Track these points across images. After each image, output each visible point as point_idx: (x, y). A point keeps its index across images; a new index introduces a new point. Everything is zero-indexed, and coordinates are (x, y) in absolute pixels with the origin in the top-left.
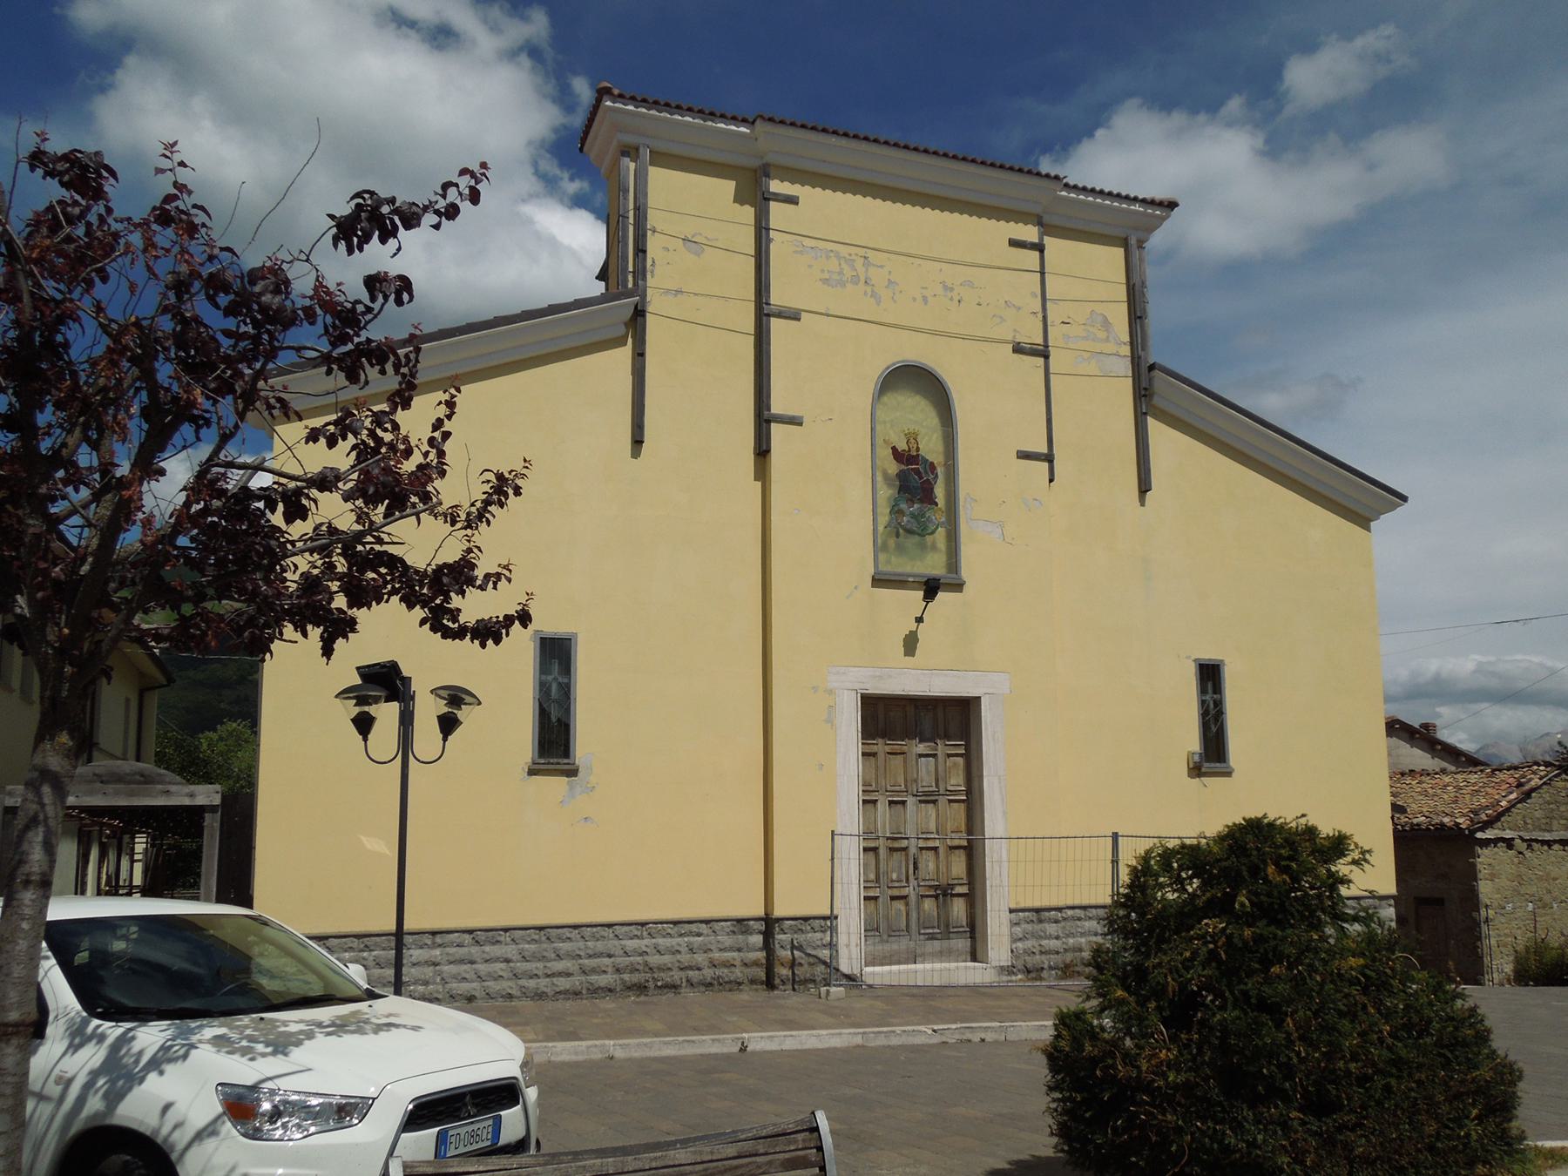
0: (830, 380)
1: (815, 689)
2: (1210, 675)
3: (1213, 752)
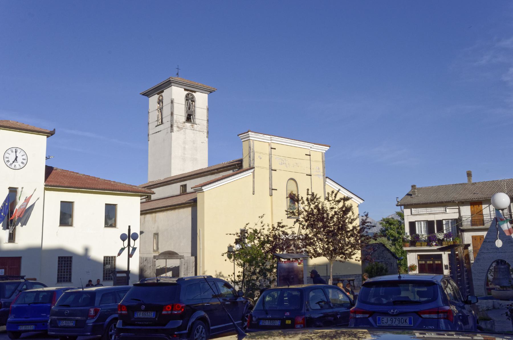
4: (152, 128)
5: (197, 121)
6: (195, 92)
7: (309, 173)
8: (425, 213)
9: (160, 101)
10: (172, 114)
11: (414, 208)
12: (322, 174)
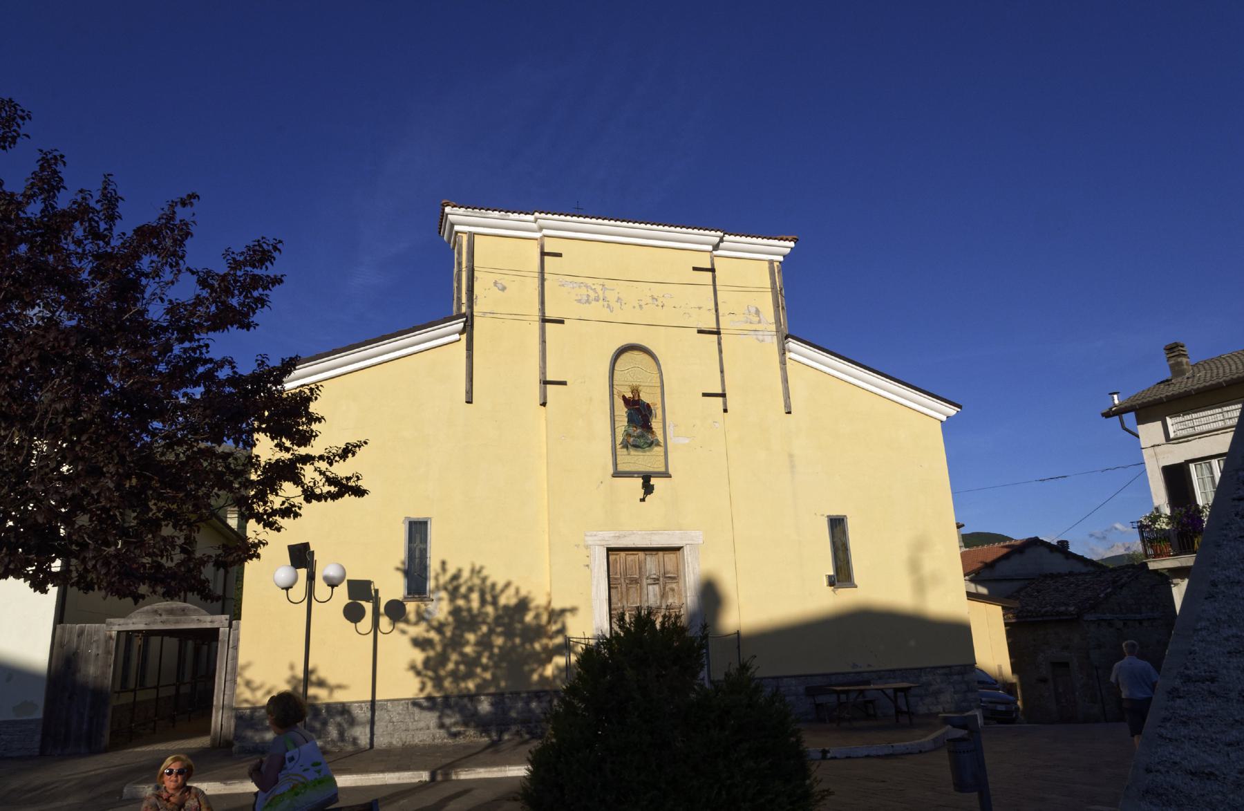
0: (583, 360)
1: (577, 546)
2: (837, 525)
3: (842, 575)
7: (712, 325)
8: (1221, 424)
11: (1175, 414)
12: (773, 327)
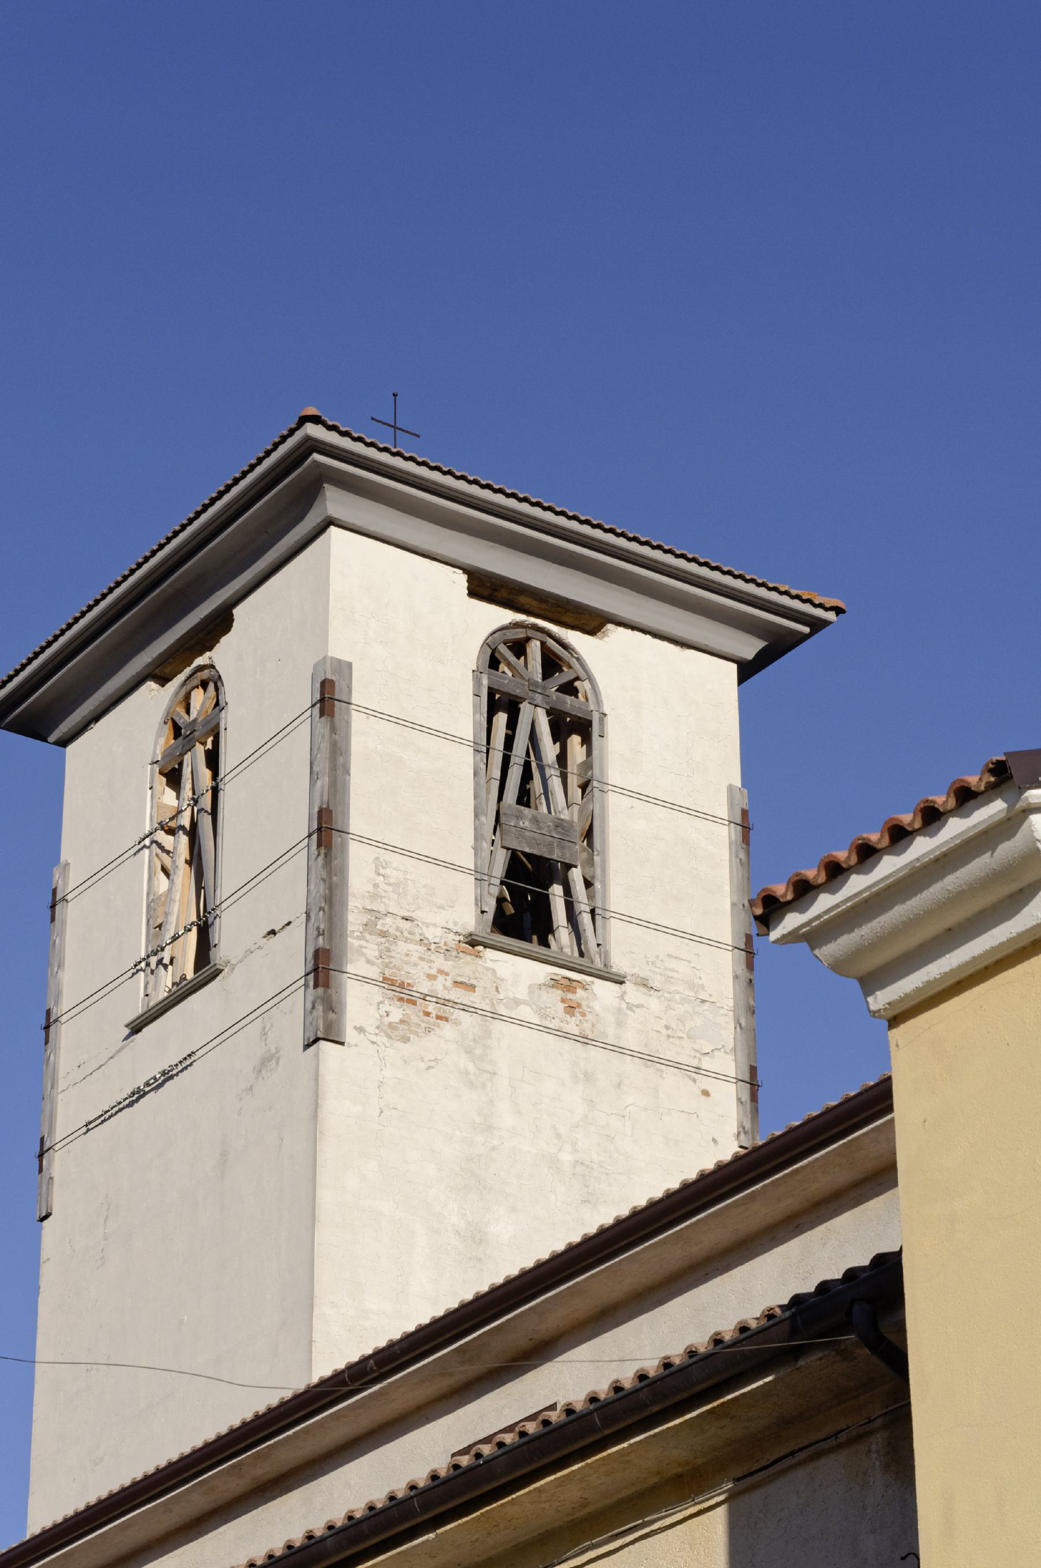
4: (89, 1059)
5: (622, 945)
6: (592, 622)
9: (194, 747)
10: (326, 831)
